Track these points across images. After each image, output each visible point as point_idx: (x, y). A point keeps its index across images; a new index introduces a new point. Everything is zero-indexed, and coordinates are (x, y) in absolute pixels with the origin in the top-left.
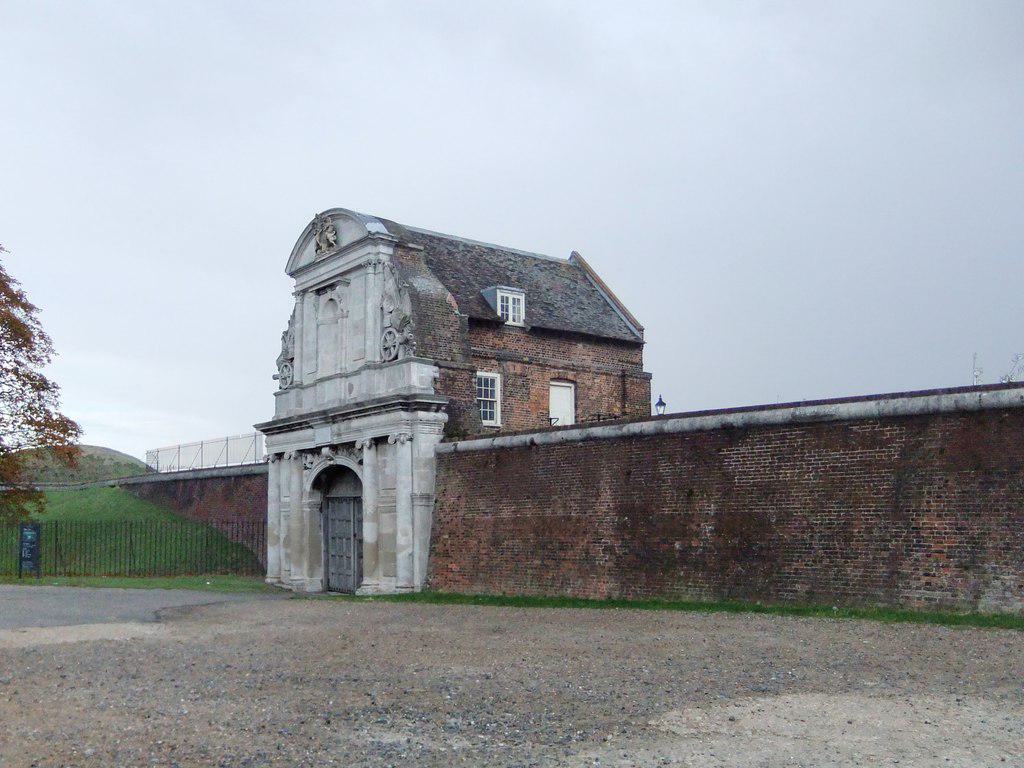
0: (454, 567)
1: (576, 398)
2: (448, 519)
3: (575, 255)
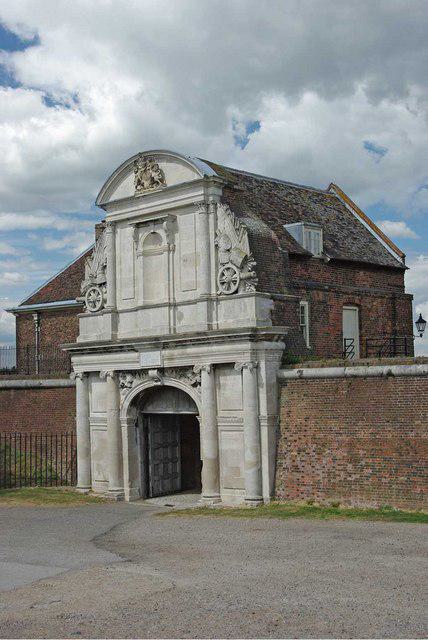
0: (307, 480)
1: (360, 320)
2: (295, 437)
3: (332, 186)
